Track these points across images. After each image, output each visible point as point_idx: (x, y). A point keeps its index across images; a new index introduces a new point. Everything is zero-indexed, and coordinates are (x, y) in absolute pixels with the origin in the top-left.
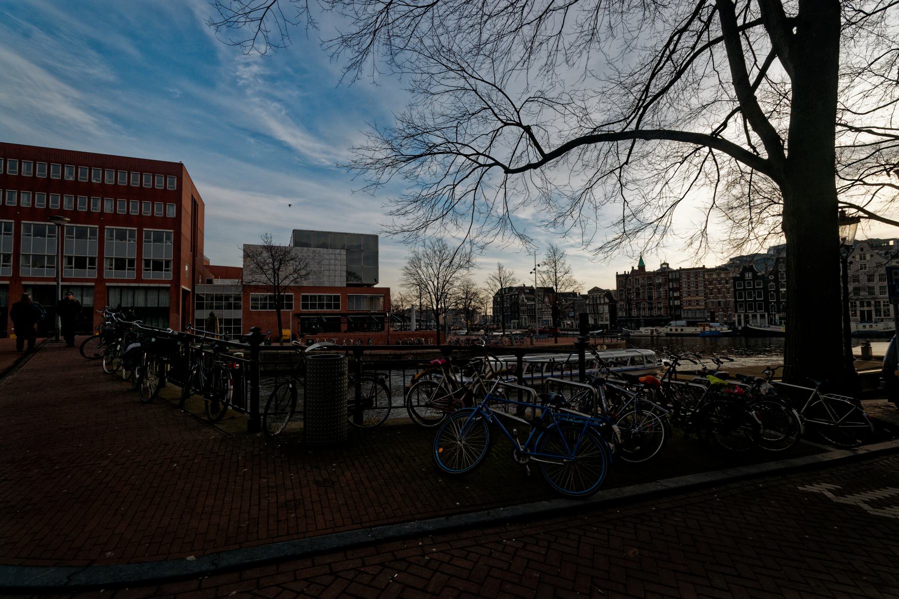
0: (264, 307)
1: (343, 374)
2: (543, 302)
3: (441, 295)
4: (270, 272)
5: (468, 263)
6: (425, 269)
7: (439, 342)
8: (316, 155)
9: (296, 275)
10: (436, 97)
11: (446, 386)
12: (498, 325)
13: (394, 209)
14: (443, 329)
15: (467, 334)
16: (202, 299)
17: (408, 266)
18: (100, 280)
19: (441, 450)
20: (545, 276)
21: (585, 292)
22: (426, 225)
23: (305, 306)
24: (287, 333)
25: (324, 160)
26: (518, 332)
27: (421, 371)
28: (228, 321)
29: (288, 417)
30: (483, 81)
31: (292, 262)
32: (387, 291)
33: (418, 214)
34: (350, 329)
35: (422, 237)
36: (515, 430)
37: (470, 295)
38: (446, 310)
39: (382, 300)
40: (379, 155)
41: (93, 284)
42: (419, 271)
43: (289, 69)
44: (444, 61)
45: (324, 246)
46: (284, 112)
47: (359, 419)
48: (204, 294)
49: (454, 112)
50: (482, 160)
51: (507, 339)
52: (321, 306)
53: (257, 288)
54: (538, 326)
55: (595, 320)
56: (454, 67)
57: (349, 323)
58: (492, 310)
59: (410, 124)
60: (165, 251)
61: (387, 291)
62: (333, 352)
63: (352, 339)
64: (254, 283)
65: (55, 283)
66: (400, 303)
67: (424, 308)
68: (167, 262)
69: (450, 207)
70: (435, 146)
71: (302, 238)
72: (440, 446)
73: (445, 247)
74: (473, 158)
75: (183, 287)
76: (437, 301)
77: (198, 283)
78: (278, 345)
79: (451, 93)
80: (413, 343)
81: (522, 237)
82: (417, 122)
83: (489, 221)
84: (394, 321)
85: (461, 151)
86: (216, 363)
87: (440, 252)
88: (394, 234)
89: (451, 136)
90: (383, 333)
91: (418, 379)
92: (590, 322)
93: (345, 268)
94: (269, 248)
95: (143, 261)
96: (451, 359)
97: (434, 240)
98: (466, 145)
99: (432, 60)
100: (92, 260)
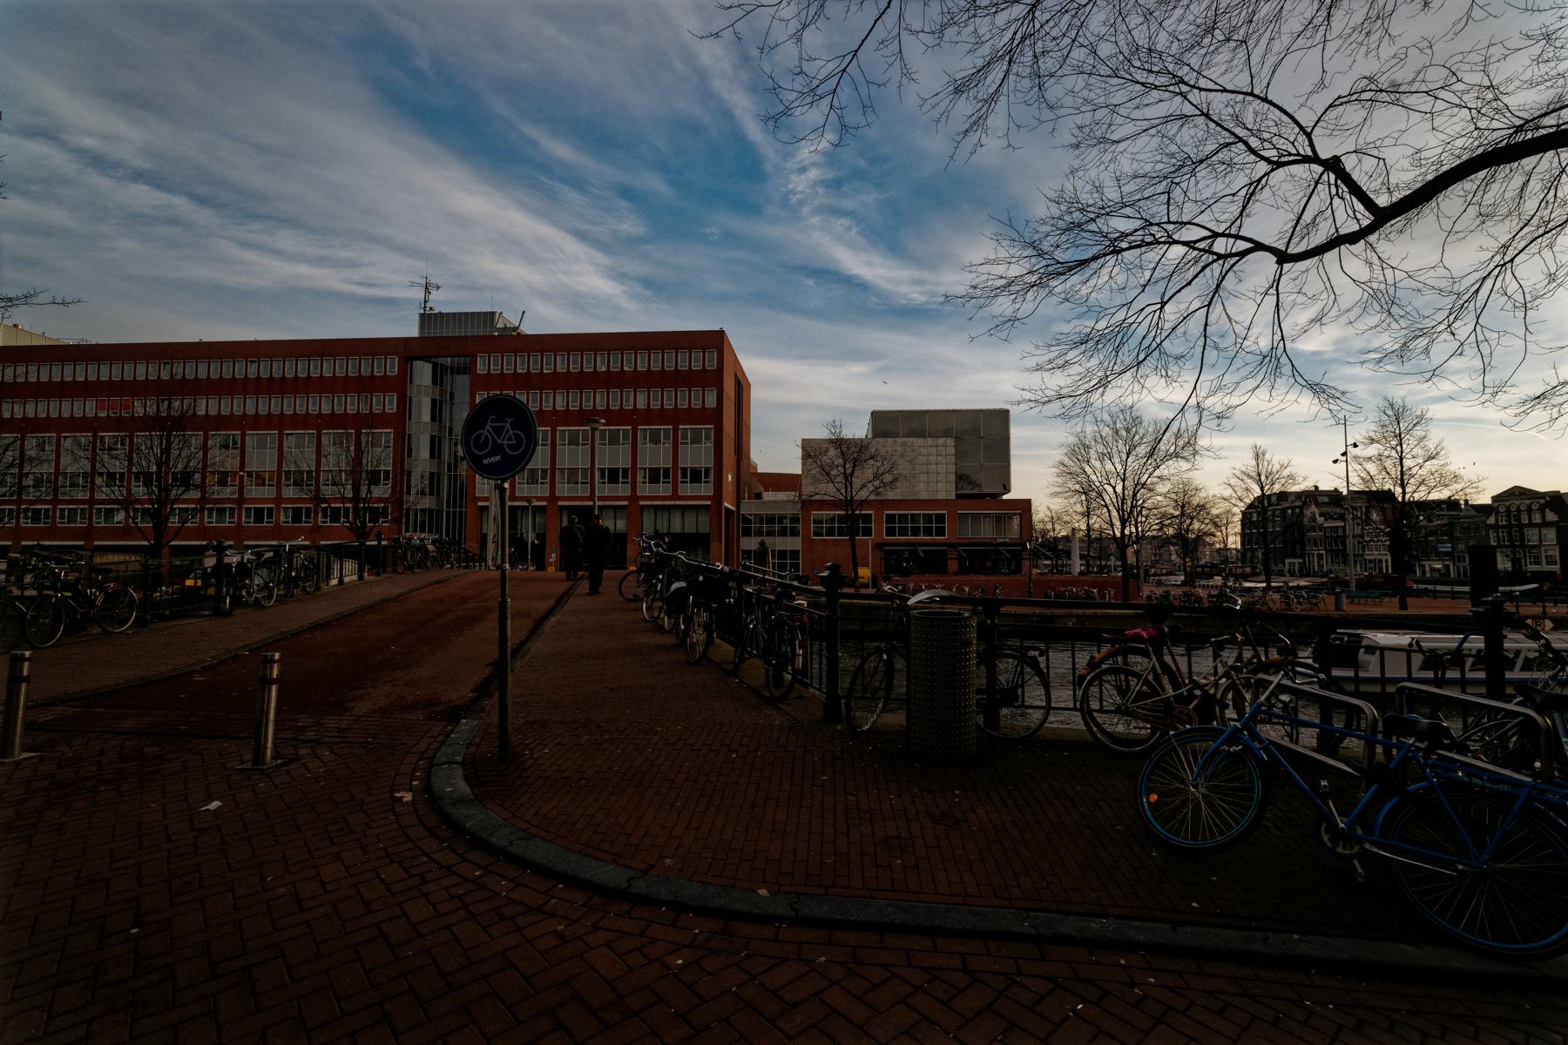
0: (831, 532)
1: (970, 644)
2: (1368, 521)
3: (1128, 512)
4: (840, 479)
5: (1188, 447)
6: (1097, 464)
7: (1126, 596)
8: (903, 289)
9: (877, 483)
10: (1121, 146)
11: (1157, 678)
12: (1254, 568)
13: (1043, 359)
14: (1131, 576)
15: (1184, 584)
16: (749, 521)
17: (1066, 460)
18: (634, 498)
19: (1154, 797)
20: (1372, 468)
21: (1485, 499)
22: (1103, 383)
23: (891, 532)
24: (865, 573)
25: (915, 295)
26: (1302, 583)
27: (1106, 649)
28: (782, 554)
29: (880, 706)
30: (1225, 90)
31: (871, 462)
33: (1088, 365)
34: (963, 570)
35: (1098, 404)
36: (1324, 783)
37: (1188, 507)
38: (1139, 539)
39: (1016, 521)
40: (1015, 271)
41: (626, 503)
42: (1088, 469)
43: (862, 163)
44: (1140, 76)
45: (922, 434)
47: (993, 720)
48: (750, 515)
49: (1159, 166)
50: (1220, 246)
51: (1277, 596)
52: (916, 532)
53: (822, 504)
54: (1353, 573)
55: (1515, 562)
56: (1163, 80)
57: (961, 560)
58: (1238, 539)
59: (1076, 204)
60: (698, 455)
62: (950, 609)
63: (968, 586)
65: (590, 503)
66: (1049, 526)
67: (1094, 535)
68: (707, 470)
69: (1154, 345)
70: (1124, 235)
71: (884, 423)
72: (1149, 792)
73: (1137, 421)
74: (1202, 245)
75: (726, 504)
76: (1123, 522)
77: (744, 499)
78: (851, 591)
79: (1153, 131)
80: (1077, 597)
81: (1317, 389)
82: (1086, 198)
83: (1238, 363)
84: (1039, 558)
85: (1176, 237)
86: (780, 614)
87: (1128, 431)
88: (1044, 403)
89: (1157, 210)
91: (1102, 661)
92: (1500, 566)
93: (952, 468)
94: (839, 443)
96: (1166, 630)
97: (1115, 410)
98: (1186, 224)
99: (1115, 81)
100: (625, 471)
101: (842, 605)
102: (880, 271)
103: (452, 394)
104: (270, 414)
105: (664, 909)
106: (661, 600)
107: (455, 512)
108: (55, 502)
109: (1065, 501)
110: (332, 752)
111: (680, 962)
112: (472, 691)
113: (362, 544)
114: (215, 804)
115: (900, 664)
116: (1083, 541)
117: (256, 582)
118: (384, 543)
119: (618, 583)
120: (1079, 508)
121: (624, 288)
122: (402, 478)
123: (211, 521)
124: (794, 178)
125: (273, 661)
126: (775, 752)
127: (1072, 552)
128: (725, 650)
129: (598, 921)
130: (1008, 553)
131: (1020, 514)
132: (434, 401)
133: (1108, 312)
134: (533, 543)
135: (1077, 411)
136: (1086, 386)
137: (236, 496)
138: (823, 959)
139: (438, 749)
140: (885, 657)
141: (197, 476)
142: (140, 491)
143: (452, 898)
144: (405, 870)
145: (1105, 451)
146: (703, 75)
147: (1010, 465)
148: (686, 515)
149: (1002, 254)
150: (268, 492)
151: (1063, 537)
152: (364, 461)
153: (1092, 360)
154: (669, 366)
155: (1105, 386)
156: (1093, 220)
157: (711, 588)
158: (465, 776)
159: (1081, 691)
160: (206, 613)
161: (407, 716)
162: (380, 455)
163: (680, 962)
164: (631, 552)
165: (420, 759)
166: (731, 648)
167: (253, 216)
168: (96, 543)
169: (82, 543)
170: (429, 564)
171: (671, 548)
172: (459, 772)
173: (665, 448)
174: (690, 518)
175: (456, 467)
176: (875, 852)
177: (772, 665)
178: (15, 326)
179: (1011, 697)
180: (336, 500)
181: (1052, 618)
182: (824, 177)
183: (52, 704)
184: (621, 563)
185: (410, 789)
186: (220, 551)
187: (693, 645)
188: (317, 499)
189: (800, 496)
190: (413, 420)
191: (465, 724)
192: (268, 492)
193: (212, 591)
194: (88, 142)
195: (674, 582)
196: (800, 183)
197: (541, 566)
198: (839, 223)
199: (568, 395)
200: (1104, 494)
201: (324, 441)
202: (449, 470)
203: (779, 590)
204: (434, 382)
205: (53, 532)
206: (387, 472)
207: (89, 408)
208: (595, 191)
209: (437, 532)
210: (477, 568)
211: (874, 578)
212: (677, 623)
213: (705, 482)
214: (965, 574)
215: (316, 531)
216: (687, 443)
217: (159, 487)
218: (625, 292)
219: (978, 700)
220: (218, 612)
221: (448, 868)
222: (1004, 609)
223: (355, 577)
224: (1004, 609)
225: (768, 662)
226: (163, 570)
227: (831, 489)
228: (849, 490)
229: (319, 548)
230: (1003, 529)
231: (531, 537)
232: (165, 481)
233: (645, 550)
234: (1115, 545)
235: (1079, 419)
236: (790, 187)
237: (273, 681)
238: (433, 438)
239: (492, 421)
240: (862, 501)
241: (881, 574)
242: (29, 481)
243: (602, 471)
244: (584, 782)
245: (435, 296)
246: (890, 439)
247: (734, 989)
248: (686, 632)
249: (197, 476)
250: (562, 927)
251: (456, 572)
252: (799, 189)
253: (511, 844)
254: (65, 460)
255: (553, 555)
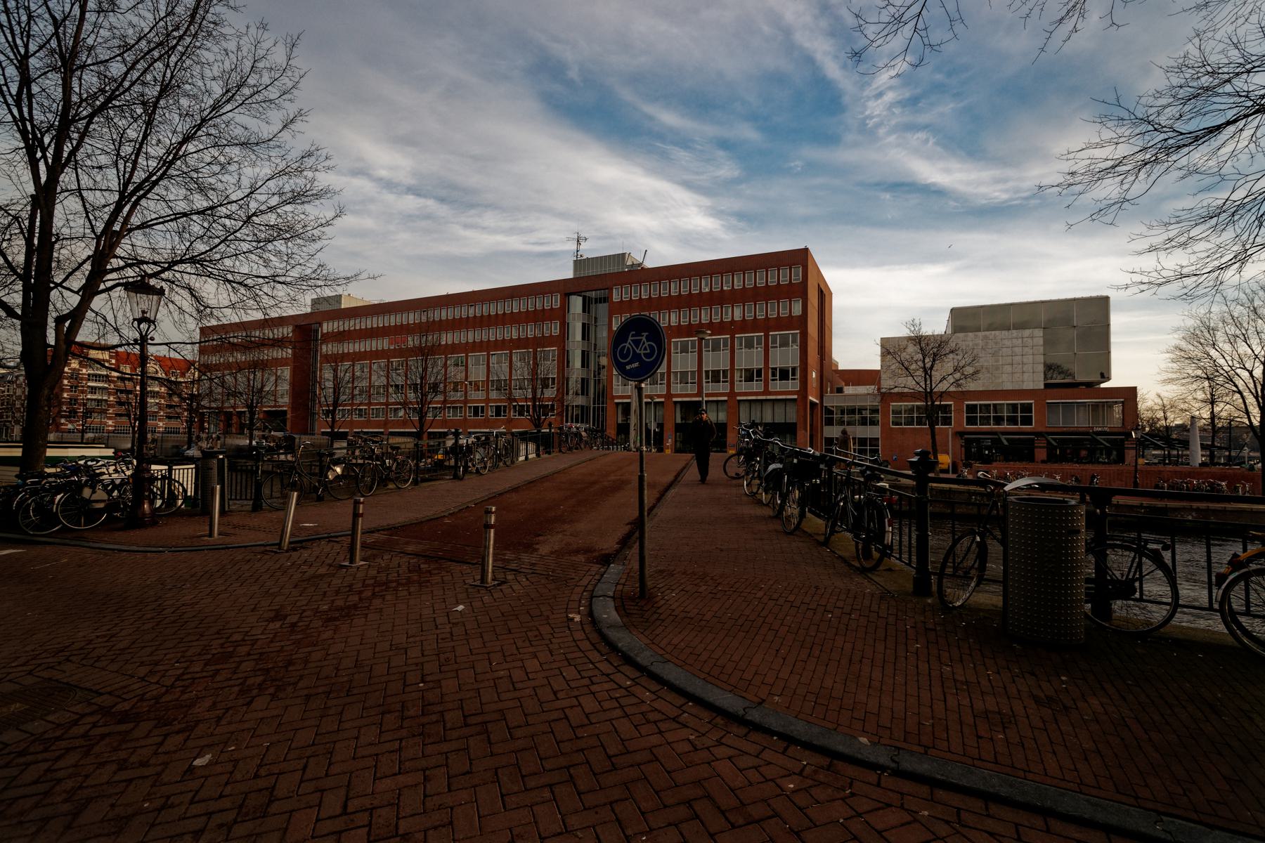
1: (1078, 532)
4: (920, 373)
6: (1227, 347)
8: (983, 190)
9: (958, 375)
16: (831, 412)
17: (1184, 345)
18: (732, 394)
25: (997, 194)
27: (1253, 548)
28: (863, 442)
29: (973, 584)
31: (951, 356)
32: (1130, 393)
33: (1219, 241)
34: (1052, 458)
39: (1117, 409)
40: (1123, 150)
41: (726, 398)
42: (1213, 352)
43: (939, 77)
46: (932, 141)
47: (1103, 610)
48: (833, 407)
52: (998, 420)
53: (901, 396)
57: (1050, 449)
60: (786, 357)
61: (1130, 393)
64: (896, 390)
65: (701, 399)
66: (1160, 414)
68: (794, 369)
71: (963, 318)
75: (811, 398)
84: (1147, 447)
86: (869, 494)
90: (1120, 467)
91: (1250, 560)
93: (1041, 359)
94: (918, 340)
95: (770, 371)
101: (932, 489)
102: (959, 176)
103: (596, 318)
104: (489, 340)
105: (775, 738)
106: (759, 477)
107: (599, 407)
108: (370, 404)
109: (1182, 388)
110: (527, 579)
111: (792, 786)
112: (617, 543)
113: (539, 431)
114: (461, 608)
115: (995, 548)
116: (1205, 430)
117: (477, 457)
118: (553, 430)
119: (723, 463)
120: (1200, 395)
121: (722, 222)
122: (563, 384)
123: (450, 415)
124: (871, 104)
125: (491, 512)
126: (868, 616)
127: (1191, 443)
128: (816, 523)
129: (722, 738)
130: (1107, 442)
131: (1122, 402)
132: (584, 325)
133: (1249, 178)
134: (655, 430)
135: (1201, 291)
136: (1217, 263)
137: (463, 398)
138: (926, 813)
139: (596, 585)
140: (978, 539)
141: (442, 385)
142: (411, 396)
143: (612, 698)
144: (579, 672)
145: (1238, 332)
146: (787, 32)
147: (1109, 352)
148: (764, 406)
149: (1107, 134)
150: (481, 395)
151: (1178, 426)
152: (539, 371)
153: (1224, 234)
154: (761, 283)
155: (1243, 262)
156: (1229, 81)
157: (804, 469)
158: (616, 607)
159: (1221, 592)
160: (448, 477)
161: (574, 558)
162: (549, 367)
163: (792, 786)
164: (731, 438)
165: (584, 591)
166: (820, 521)
167: (472, 206)
168: (390, 430)
169: (382, 430)
170: (582, 446)
171: (767, 435)
172: (611, 604)
173: (758, 352)
174: (779, 410)
175: (599, 374)
176: (975, 722)
177: (861, 539)
178: (349, 295)
179: (1126, 589)
180: (521, 400)
181: (1165, 510)
182: (901, 97)
183: (373, 532)
184: (722, 447)
185: (579, 613)
186: (456, 435)
187: (788, 518)
188: (511, 399)
189: (879, 389)
190: (570, 340)
191: (613, 568)
192: (481, 395)
193: (452, 462)
194: (383, 173)
195: (770, 464)
196: (876, 108)
197: (661, 450)
198: (915, 137)
199: (680, 313)
200: (1237, 380)
201: (514, 359)
202: (595, 376)
203: (868, 472)
204: (584, 311)
205: (368, 423)
206: (553, 379)
207: (383, 344)
208: (698, 147)
209: (587, 423)
210: (615, 450)
211: (954, 464)
212: (773, 498)
213: (792, 379)
214: (1056, 462)
215: (510, 421)
216: (776, 347)
217: (422, 393)
218: (723, 226)
219: (1087, 589)
220: (456, 477)
221: (608, 675)
222: (1115, 500)
223: (534, 455)
224: (1115, 500)
225: (857, 536)
226: (424, 448)
227: (910, 382)
228: (928, 382)
229: (513, 434)
230: (1101, 418)
231: (653, 427)
232: (426, 389)
233: (743, 437)
234: (1251, 434)
235: (1207, 298)
236: (867, 113)
237: (491, 527)
238: (583, 352)
239: (633, 336)
240: (942, 393)
241: (962, 460)
242: (356, 392)
243: (707, 372)
244: (704, 623)
245: (584, 246)
246: (970, 334)
247: (841, 821)
248: (782, 507)
249: (442, 385)
250: (693, 737)
251: (601, 452)
252: (875, 113)
253: (652, 664)
254: (374, 378)
255: (670, 440)
